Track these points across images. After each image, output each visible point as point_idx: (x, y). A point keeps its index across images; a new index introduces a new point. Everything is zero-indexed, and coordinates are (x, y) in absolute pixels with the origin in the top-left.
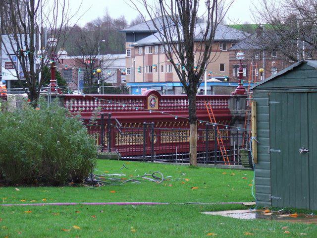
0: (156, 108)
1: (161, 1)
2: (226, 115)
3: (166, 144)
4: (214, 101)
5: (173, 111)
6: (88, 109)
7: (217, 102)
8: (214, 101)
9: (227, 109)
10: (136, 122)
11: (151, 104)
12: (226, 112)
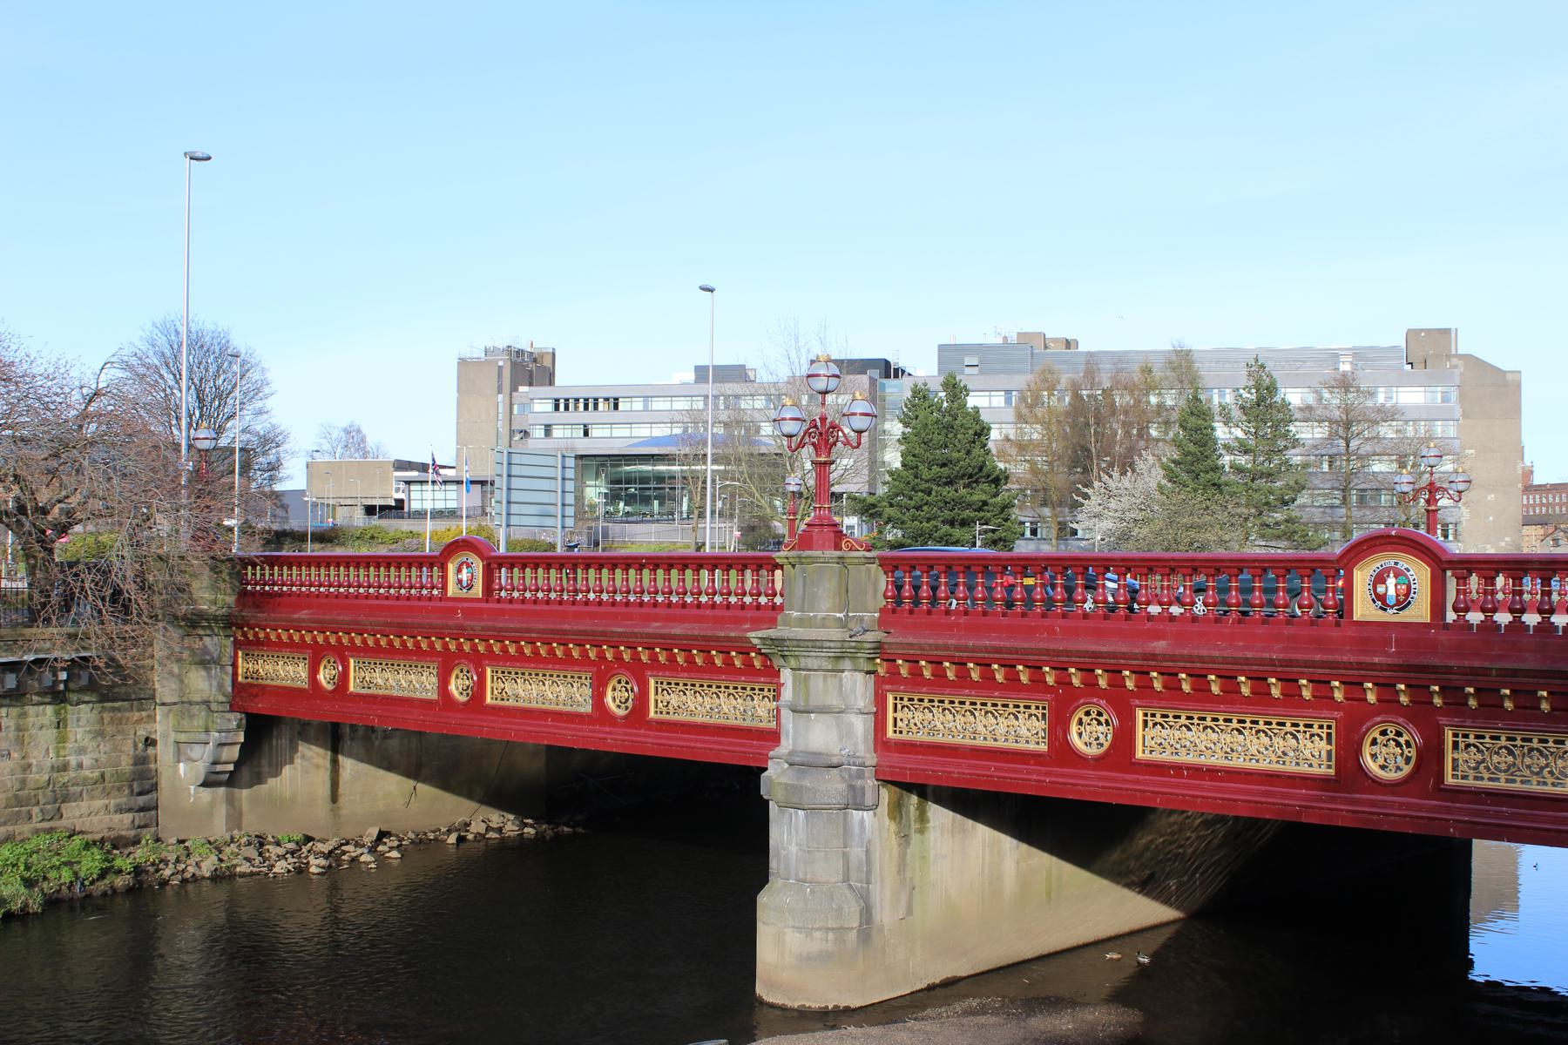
11: (1382, 598)
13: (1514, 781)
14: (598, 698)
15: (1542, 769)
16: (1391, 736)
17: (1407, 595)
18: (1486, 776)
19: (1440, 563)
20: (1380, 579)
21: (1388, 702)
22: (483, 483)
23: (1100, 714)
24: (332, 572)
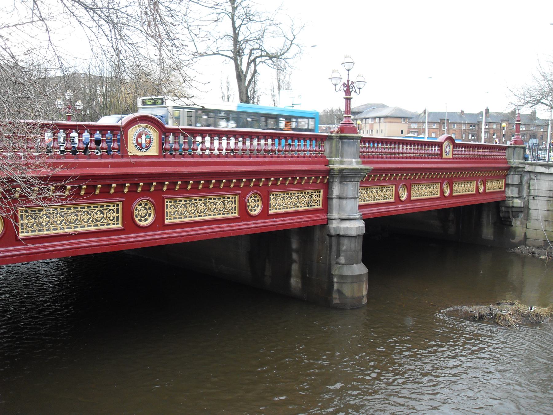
0: (154, 151)
1: (35, 2)
2: (322, 167)
3: (29, 240)
4: (405, 147)
5: (460, 160)
6: (207, 152)
7: (412, 147)
8: (405, 147)
9: (505, 159)
10: (389, 173)
11: (140, 145)
12: (503, 163)
13: (77, 227)
14: (243, 207)
15: (88, 220)
16: (143, 205)
17: (150, 143)
18: (92, 224)
19: (164, 131)
20: (140, 136)
21: (146, 191)
22: (201, 55)
23: (146, 204)
24: (433, 149)
